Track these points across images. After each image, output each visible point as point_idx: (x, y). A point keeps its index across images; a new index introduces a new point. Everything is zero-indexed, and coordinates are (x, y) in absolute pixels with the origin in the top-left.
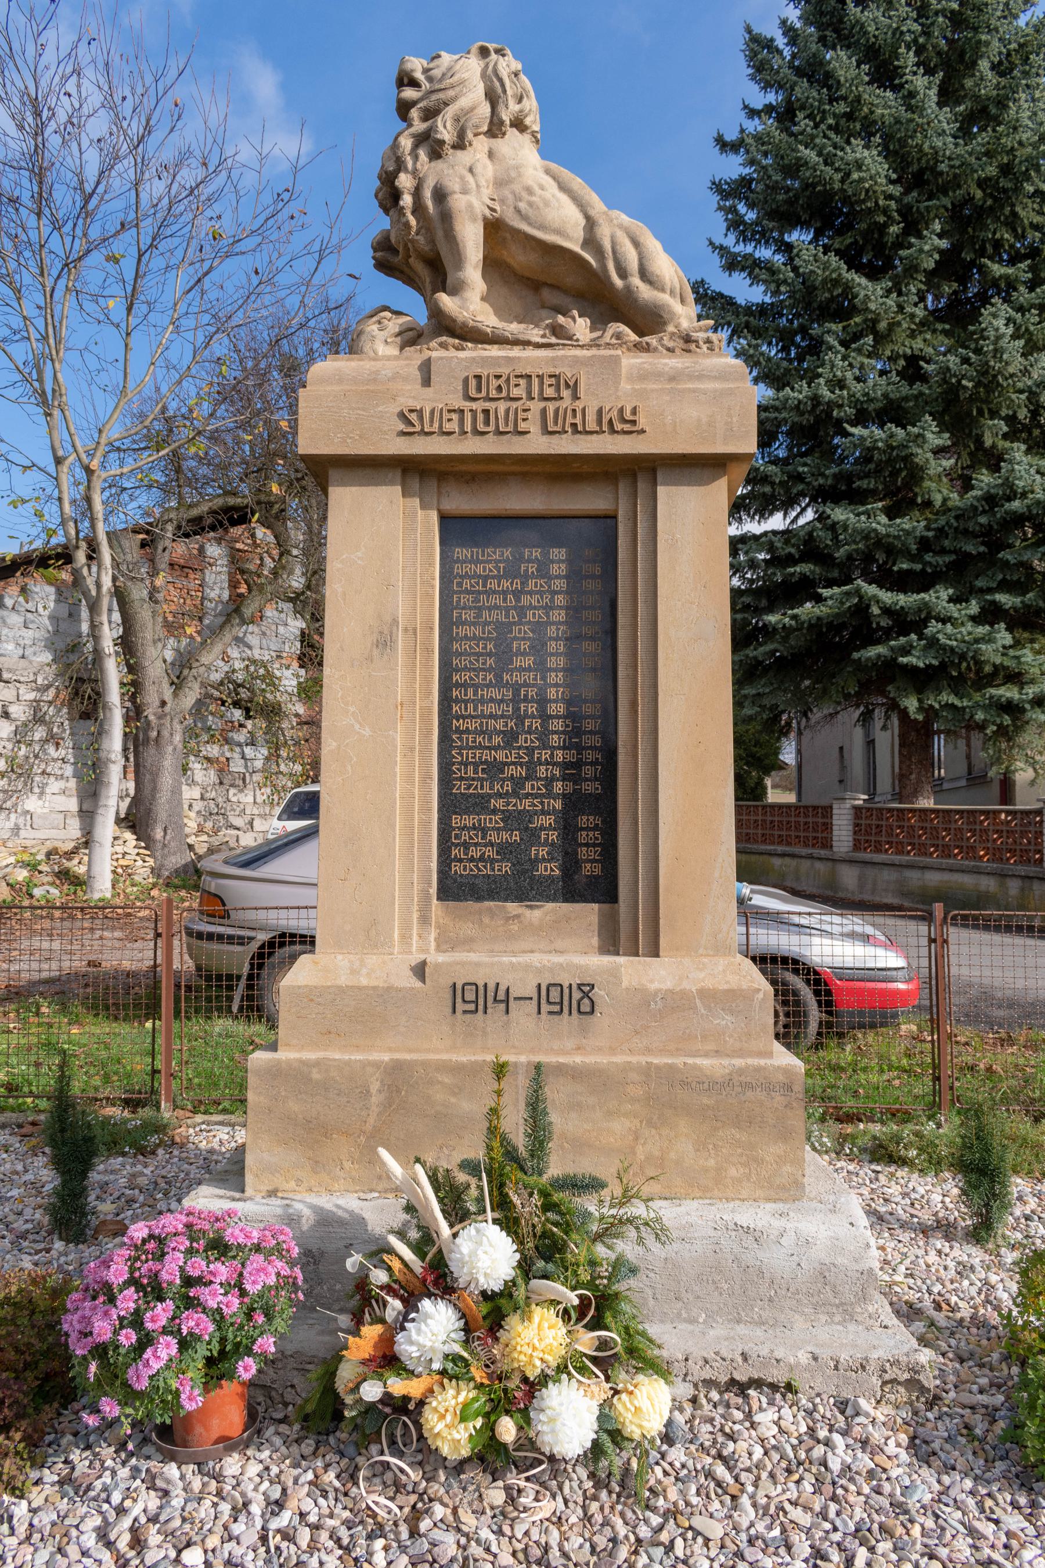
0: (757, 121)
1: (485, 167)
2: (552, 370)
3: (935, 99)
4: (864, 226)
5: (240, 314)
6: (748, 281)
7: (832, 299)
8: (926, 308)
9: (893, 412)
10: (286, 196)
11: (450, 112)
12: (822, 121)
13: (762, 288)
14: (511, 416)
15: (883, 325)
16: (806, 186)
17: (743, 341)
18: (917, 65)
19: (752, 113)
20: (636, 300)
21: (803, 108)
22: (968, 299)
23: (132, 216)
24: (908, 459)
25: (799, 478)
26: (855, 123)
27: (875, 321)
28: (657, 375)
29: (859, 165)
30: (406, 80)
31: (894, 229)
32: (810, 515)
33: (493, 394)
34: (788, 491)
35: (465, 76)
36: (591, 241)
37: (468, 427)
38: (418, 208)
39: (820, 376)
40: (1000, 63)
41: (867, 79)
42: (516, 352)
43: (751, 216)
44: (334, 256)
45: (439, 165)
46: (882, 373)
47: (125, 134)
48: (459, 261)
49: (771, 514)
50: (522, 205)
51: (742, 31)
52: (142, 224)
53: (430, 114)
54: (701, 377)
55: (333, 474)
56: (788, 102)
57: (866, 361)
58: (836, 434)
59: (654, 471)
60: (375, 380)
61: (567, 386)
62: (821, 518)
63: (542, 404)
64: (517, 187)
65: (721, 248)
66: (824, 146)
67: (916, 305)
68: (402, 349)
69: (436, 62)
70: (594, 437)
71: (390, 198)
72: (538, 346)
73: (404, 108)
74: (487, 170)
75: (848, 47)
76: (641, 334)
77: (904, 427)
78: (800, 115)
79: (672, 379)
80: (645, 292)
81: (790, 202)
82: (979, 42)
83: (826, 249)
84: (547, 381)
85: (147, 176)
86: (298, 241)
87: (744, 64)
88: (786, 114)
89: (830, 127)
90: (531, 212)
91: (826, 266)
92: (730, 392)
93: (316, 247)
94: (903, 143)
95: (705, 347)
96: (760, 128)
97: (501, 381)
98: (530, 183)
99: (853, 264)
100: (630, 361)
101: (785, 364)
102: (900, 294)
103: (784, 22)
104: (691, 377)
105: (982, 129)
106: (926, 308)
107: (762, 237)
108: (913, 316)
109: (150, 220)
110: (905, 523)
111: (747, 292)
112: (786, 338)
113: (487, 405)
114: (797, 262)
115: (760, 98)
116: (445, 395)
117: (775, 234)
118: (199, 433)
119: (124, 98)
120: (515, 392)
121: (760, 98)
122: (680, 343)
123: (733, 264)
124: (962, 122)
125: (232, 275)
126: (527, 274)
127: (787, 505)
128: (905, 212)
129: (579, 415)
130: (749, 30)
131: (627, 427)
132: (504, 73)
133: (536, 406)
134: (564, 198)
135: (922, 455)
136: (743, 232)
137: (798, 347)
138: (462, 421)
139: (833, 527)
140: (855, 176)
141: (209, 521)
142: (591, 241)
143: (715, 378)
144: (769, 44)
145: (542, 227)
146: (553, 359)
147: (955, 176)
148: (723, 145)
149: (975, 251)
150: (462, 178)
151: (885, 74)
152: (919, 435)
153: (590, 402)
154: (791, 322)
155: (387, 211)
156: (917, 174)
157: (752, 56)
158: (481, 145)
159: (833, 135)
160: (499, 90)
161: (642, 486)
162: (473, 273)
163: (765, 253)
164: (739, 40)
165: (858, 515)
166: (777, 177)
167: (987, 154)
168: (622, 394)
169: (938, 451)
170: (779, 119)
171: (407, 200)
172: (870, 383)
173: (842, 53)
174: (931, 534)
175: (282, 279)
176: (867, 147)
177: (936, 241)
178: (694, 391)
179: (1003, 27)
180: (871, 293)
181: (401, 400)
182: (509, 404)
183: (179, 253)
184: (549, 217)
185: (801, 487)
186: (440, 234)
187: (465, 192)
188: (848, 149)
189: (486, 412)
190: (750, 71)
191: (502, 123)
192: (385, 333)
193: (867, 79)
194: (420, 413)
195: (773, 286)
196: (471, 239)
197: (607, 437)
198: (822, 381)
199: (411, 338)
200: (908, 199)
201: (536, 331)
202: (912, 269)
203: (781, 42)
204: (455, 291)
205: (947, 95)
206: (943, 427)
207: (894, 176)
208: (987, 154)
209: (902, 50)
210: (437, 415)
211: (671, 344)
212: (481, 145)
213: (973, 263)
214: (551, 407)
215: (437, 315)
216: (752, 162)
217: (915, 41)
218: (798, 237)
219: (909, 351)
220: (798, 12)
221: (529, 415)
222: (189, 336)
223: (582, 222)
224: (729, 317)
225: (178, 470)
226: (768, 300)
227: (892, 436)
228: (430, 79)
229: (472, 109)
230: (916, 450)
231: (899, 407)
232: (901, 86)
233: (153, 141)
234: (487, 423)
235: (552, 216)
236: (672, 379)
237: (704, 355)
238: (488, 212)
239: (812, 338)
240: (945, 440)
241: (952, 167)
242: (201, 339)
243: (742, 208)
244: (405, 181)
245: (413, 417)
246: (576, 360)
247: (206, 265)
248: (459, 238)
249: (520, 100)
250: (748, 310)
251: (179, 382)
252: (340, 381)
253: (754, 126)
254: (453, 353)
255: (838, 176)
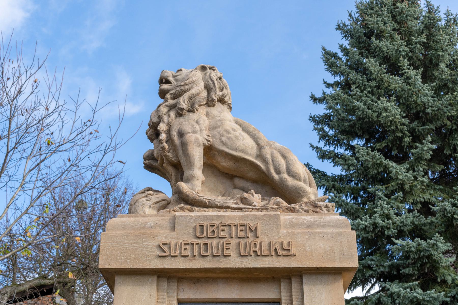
0: (331, 89)
1: (204, 121)
2: (242, 222)
3: (420, 80)
4: (391, 138)
5: (58, 181)
6: (332, 164)
7: (378, 173)
8: (429, 178)
9: (417, 232)
10: (88, 124)
11: (187, 95)
12: (365, 89)
13: (341, 168)
14: (220, 247)
15: (407, 187)
16: (359, 119)
17: (331, 194)
18: (410, 65)
19: (328, 85)
20: (286, 185)
21: (354, 83)
22: (450, 174)
23: (6, 133)
24: (429, 257)
25: (369, 267)
26: (382, 91)
27: (403, 185)
28: (300, 225)
29: (386, 110)
30: (164, 80)
31: (407, 140)
32: (377, 288)
33: (210, 235)
34: (363, 275)
35: (195, 79)
36: (260, 156)
37: (196, 253)
38: (169, 140)
39: (376, 212)
40: (450, 64)
41: (385, 71)
42: (222, 213)
43: (331, 133)
44: (112, 152)
45: (181, 119)
46: (410, 211)
47: (7, 94)
48: (191, 165)
49: (355, 287)
50: (224, 139)
51: (321, 50)
52: (11, 137)
53: (176, 96)
54: (324, 226)
55: (118, 280)
56: (347, 80)
57: (400, 205)
58: (387, 243)
59: (301, 277)
60: (144, 227)
61: (251, 230)
62: (383, 289)
63: (237, 240)
64: (221, 130)
65: (317, 148)
66: (367, 100)
67: (423, 176)
68: (159, 210)
69: (179, 73)
70: (267, 258)
71: (154, 134)
72: (234, 209)
73: (163, 94)
74: (206, 122)
75: (374, 57)
76: (289, 202)
77: (425, 240)
78: (353, 87)
79: (309, 227)
80: (291, 181)
81: (351, 126)
82: (439, 55)
83: (373, 149)
84: (240, 228)
85: (16, 114)
86: (93, 145)
87: (323, 64)
88: (346, 86)
89: (369, 92)
90: (228, 142)
91: (374, 157)
92: (341, 234)
93: (103, 147)
94: (407, 99)
95: (325, 210)
96: (333, 92)
97: (214, 228)
98: (228, 128)
99: (387, 156)
100: (285, 217)
101: (356, 206)
102: (414, 171)
103: (341, 46)
104: (319, 226)
105: (446, 93)
106: (429, 178)
107: (339, 143)
108: (422, 182)
109: (15, 135)
110: (432, 293)
111: (332, 169)
112: (355, 194)
113: (206, 241)
114: (358, 155)
115: (332, 79)
116: (184, 235)
117: (345, 141)
118: (30, 244)
119: (8, 79)
120: (222, 234)
121: (332, 79)
122: (312, 208)
123: (323, 156)
124: (435, 90)
125: (56, 162)
126: (226, 172)
127: (364, 282)
128: (412, 132)
129: (258, 246)
130: (324, 49)
131: (285, 253)
132: (214, 79)
133: (234, 242)
134: (245, 135)
135: (437, 255)
136: (328, 140)
137: (362, 197)
138: (192, 249)
139: (391, 296)
140: (384, 114)
141: (28, 293)
142: (260, 156)
143: (332, 226)
144: (334, 55)
145: (234, 149)
146: (243, 216)
147: (435, 115)
148: (315, 99)
149: (451, 150)
150: (193, 126)
151: (394, 69)
152: (434, 245)
153: (265, 239)
154: (357, 184)
155: (152, 141)
156: (416, 113)
157: (327, 61)
158: (202, 110)
159: (371, 96)
160: (212, 85)
161: (295, 285)
162: (198, 171)
163: (340, 150)
164: (320, 53)
165: (405, 288)
166: (344, 115)
167: (450, 105)
168: (282, 235)
169: (446, 252)
170: (342, 88)
171: (163, 136)
172: (404, 216)
173: (372, 60)
174: (448, 299)
175: (82, 164)
176: (389, 101)
177: (430, 145)
178: (321, 233)
179: (449, 49)
180: (398, 170)
181: (159, 238)
182: (219, 240)
183: (29, 151)
184: (238, 144)
185: (371, 272)
186: (181, 152)
187: (194, 132)
188: (379, 102)
189: (206, 244)
190: (326, 67)
191: (213, 100)
192: (150, 202)
193: (385, 71)
194: (169, 245)
195: (346, 167)
196: (197, 155)
197: (275, 258)
198: (377, 215)
199: (164, 205)
200: (413, 125)
201: (231, 201)
202: (419, 159)
203: (340, 54)
204: (187, 181)
205: (426, 78)
206: (447, 240)
207: (404, 115)
208: (450, 105)
209: (401, 59)
210: (178, 246)
211: (306, 208)
212: (202, 110)
213: (450, 155)
214: (242, 242)
215: (178, 193)
216: (330, 108)
217: (407, 55)
218: (357, 142)
219: (422, 200)
220: (348, 42)
221: (230, 246)
222: (30, 192)
223: (255, 146)
224: (324, 182)
225: (14, 265)
226: (344, 173)
227: (419, 245)
228: (177, 80)
229: (198, 94)
230: (434, 252)
231: (421, 229)
232: (403, 74)
233: (21, 98)
234: (207, 250)
235: (240, 144)
236: (309, 227)
237: (325, 214)
238: (206, 142)
239: (369, 193)
240: (448, 246)
241: (434, 110)
242: (35, 194)
243: (326, 129)
244: (162, 127)
245: (165, 248)
246: (255, 217)
247: (43, 157)
248: (191, 154)
249: (222, 89)
250: (334, 178)
251: (20, 217)
252: (125, 228)
253: (330, 91)
254: (187, 213)
255: (375, 115)
